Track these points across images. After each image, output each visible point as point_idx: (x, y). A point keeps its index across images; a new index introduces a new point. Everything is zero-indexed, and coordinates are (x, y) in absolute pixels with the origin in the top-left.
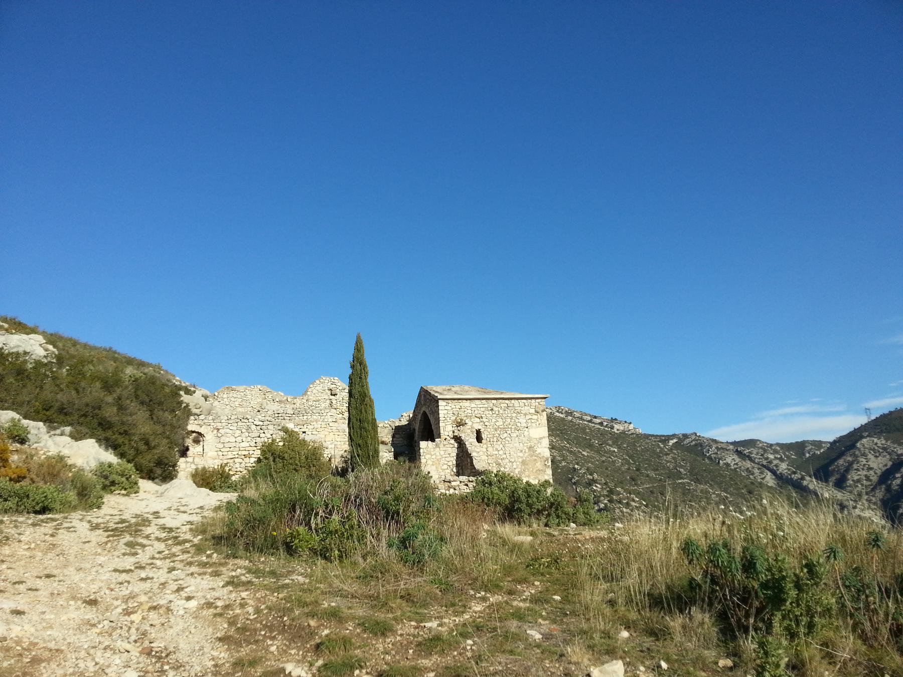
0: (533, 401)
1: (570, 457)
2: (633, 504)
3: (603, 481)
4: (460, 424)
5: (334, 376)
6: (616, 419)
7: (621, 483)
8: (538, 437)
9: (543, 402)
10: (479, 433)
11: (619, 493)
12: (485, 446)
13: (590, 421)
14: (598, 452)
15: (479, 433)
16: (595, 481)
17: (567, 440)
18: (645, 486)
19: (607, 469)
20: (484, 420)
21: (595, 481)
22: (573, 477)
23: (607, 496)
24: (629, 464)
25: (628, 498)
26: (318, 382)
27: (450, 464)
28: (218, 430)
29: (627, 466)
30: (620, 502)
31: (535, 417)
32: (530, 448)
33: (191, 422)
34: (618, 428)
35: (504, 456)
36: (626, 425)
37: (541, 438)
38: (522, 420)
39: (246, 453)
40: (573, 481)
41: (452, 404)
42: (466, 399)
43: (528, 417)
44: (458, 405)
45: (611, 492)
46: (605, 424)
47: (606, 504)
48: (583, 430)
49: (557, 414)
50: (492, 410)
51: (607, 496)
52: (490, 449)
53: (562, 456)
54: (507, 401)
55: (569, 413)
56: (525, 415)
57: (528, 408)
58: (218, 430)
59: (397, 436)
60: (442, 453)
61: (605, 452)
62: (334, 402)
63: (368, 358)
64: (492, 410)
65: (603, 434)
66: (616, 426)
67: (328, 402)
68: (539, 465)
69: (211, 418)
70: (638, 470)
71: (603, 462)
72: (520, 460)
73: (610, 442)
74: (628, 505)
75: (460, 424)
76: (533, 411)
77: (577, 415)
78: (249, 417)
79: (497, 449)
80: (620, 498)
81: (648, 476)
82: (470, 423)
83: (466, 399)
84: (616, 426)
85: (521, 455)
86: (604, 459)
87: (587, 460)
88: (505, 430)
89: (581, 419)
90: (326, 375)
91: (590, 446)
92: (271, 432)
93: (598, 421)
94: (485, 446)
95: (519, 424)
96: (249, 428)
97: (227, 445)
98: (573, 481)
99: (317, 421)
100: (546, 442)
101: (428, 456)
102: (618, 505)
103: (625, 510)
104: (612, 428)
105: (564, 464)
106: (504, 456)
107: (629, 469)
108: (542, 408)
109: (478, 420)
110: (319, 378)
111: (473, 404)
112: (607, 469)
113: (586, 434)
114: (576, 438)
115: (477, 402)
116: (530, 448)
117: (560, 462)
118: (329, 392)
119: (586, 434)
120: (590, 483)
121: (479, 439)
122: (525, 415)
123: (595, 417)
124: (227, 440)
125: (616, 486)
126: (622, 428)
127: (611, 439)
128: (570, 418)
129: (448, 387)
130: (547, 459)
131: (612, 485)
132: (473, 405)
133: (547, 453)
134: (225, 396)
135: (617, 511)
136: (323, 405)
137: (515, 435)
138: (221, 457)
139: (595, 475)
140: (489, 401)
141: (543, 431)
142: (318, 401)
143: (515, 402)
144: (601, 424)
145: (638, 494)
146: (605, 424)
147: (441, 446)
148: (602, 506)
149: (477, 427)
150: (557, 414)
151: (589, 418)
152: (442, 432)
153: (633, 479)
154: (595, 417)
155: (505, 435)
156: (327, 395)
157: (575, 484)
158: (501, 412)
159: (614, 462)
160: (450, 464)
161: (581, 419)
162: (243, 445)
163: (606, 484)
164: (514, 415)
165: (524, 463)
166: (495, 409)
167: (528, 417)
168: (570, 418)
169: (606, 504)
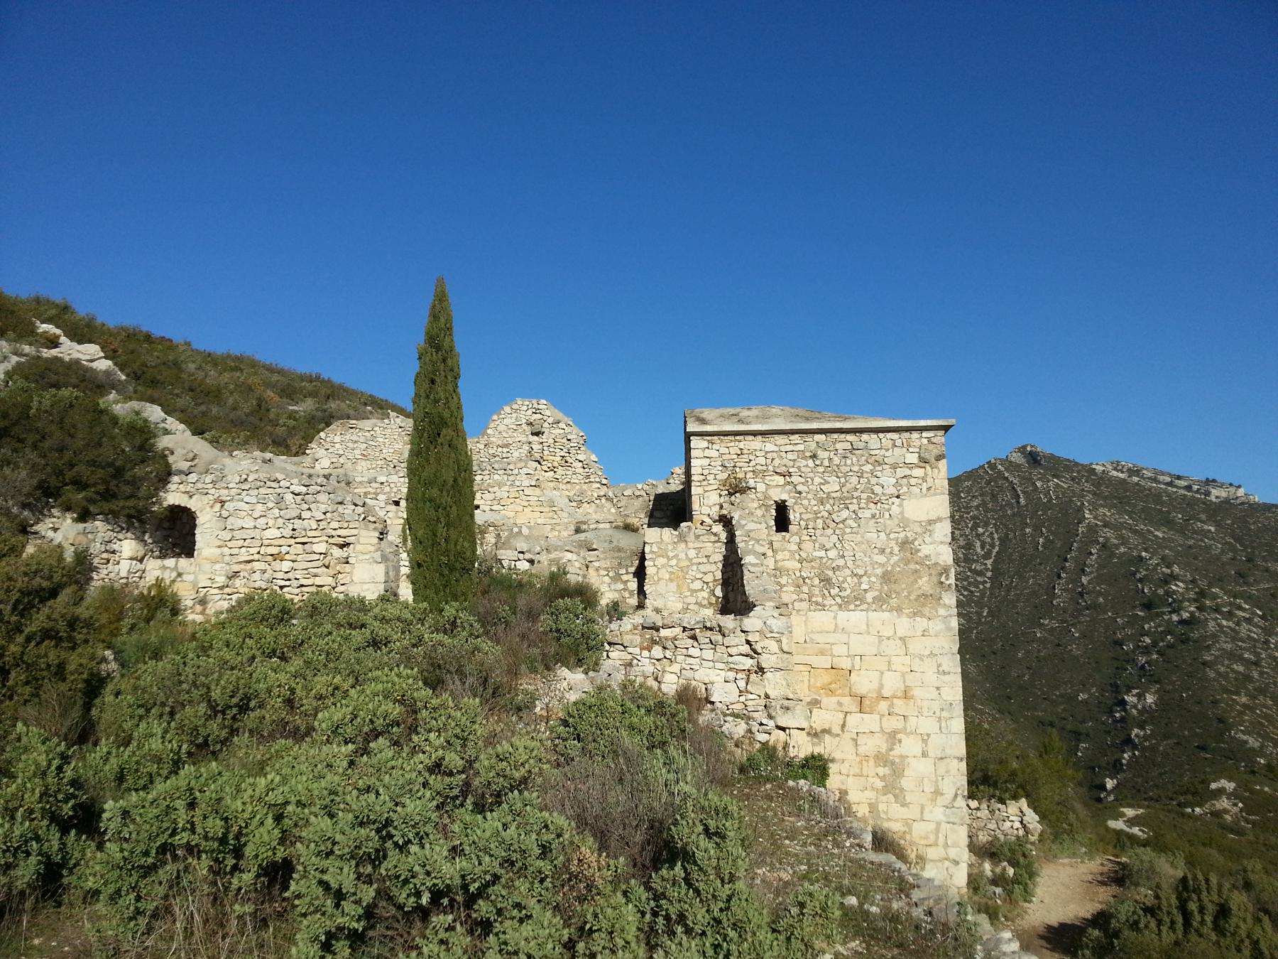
0: (915, 435)
1: (1134, 540)
2: (1241, 613)
3: (1189, 577)
4: (736, 488)
5: (538, 397)
6: (1214, 481)
7: (1220, 581)
8: (924, 518)
9: (939, 437)
10: (782, 509)
11: (1215, 597)
12: (796, 539)
13: (1170, 484)
14: (1182, 531)
15: (782, 509)
16: (1174, 577)
17: (1130, 514)
18: (1262, 586)
19: (1195, 558)
20: (795, 479)
21: (1174, 577)
22: (1137, 571)
23: (1195, 600)
24: (1234, 550)
25: (1231, 604)
26: (507, 409)
27: (709, 578)
28: (223, 503)
29: (1230, 555)
30: (1217, 610)
31: (918, 472)
32: (905, 544)
33: (172, 487)
34: (1216, 494)
35: (841, 562)
36: (1232, 490)
37: (930, 522)
38: (888, 479)
39: (274, 550)
40: (1138, 576)
41: (721, 446)
42: (755, 434)
43: (901, 472)
44: (733, 446)
45: (1202, 594)
46: (1195, 487)
47: (1192, 613)
48: (1157, 497)
49: (1115, 473)
50: (814, 456)
51: (1195, 600)
52: (808, 546)
53: (1121, 537)
54: (850, 437)
55: (1131, 472)
56: (894, 467)
57: (906, 451)
58: (223, 503)
59: (657, 514)
60: (692, 553)
61: (1195, 532)
62: (536, 447)
63: (463, 342)
64: (814, 456)
65: (1191, 503)
66: (1215, 492)
67: (526, 447)
68: (925, 584)
69: (209, 479)
70: (1249, 560)
71: (1190, 547)
72: (879, 571)
73: (1203, 517)
74: (1230, 615)
75: (736, 488)
76: (913, 458)
77: (1147, 474)
78: (280, 476)
79: (823, 547)
80: (1217, 604)
81: (1267, 570)
82: (761, 487)
83: (755, 434)
84: (1215, 492)
85: (881, 559)
86: (1191, 542)
87: (1162, 544)
88: (844, 502)
89: (1155, 480)
90: (523, 397)
91: (1169, 523)
92: (323, 507)
93: (1183, 483)
94: (796, 539)
95: (878, 489)
96: (280, 499)
97: (238, 534)
98: (1138, 576)
99: (500, 485)
100: (944, 530)
101: (661, 561)
102: (1213, 615)
103: (1224, 623)
104: (1208, 494)
105: (1122, 550)
106: (841, 562)
107: (1234, 559)
108: (936, 452)
109: (781, 480)
110: (509, 401)
111: (770, 445)
112: (1195, 558)
113: (1162, 504)
114: (1143, 510)
115: (780, 440)
116: (905, 544)
117: (1117, 547)
118: (528, 429)
119: (1162, 504)
120: (1167, 580)
121: (782, 522)
122: (894, 467)
123: (1179, 478)
124: (239, 523)
125: (1210, 585)
126: (1224, 494)
127: (1204, 511)
128: (1135, 479)
129: (732, 411)
130: (946, 571)
131: (1203, 584)
132: (770, 447)
133: (946, 555)
134: (337, 439)
135: (1211, 624)
136: (516, 454)
137: (868, 514)
138: (227, 559)
139: (1176, 569)
140: (808, 438)
141: (940, 505)
142: (507, 446)
143: (872, 439)
144: (1189, 488)
145: (1248, 598)
146: (1195, 487)
147: (691, 537)
148: (1186, 615)
149: (778, 495)
150: (1115, 473)
151: (1168, 479)
152: (695, 506)
153: (1240, 575)
154: (1179, 478)
155: (845, 514)
156: (524, 435)
157: (1140, 580)
158: (836, 460)
159: (1208, 548)
160: (709, 578)
161: (1155, 480)
162: (268, 534)
163: (1194, 581)
164: (868, 468)
165: (887, 577)
166: (821, 454)
167: (901, 472)
168: (1135, 479)
169: (1192, 613)
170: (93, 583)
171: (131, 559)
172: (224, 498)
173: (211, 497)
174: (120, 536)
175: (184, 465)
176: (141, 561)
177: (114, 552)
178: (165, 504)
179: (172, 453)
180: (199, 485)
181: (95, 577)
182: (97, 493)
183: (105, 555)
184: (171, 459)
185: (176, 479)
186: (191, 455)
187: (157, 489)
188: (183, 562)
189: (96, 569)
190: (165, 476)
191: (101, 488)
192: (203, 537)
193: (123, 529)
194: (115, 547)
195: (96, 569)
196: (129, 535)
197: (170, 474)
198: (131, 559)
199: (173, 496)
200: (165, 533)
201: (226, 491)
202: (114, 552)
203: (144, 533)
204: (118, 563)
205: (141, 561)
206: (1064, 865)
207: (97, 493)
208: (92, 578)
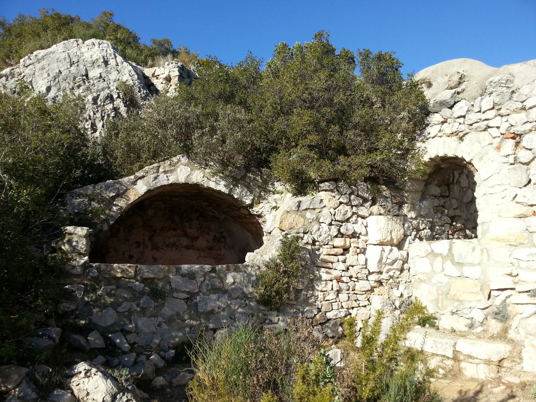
15: (322, 200)
28: (517, 137)
33: (432, 130)
58: (517, 137)
170: (320, 287)
171: (381, 244)
172: (519, 129)
173: (494, 132)
174: (363, 211)
175: (447, 95)
176: (400, 246)
177: (354, 235)
178: (426, 159)
179: (430, 85)
180: (472, 117)
181: (325, 276)
182: (311, 147)
183: (339, 242)
184: (428, 93)
185: (435, 118)
186: (456, 78)
187: (413, 140)
188: (460, 246)
189: (326, 265)
190: (420, 117)
191: (313, 138)
192: (487, 200)
193: (365, 200)
194: (359, 228)
195: (326, 265)
196: (375, 209)
197: (427, 112)
198: (381, 244)
199: (435, 145)
200: (436, 202)
201: (523, 116)
202: (354, 235)
203: (400, 205)
204: (363, 251)
205: (400, 246)
206: (131, 65)
207: (311, 147)
208: (320, 279)
